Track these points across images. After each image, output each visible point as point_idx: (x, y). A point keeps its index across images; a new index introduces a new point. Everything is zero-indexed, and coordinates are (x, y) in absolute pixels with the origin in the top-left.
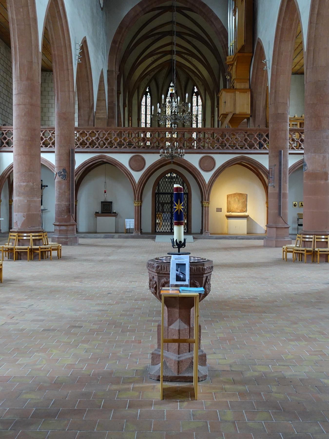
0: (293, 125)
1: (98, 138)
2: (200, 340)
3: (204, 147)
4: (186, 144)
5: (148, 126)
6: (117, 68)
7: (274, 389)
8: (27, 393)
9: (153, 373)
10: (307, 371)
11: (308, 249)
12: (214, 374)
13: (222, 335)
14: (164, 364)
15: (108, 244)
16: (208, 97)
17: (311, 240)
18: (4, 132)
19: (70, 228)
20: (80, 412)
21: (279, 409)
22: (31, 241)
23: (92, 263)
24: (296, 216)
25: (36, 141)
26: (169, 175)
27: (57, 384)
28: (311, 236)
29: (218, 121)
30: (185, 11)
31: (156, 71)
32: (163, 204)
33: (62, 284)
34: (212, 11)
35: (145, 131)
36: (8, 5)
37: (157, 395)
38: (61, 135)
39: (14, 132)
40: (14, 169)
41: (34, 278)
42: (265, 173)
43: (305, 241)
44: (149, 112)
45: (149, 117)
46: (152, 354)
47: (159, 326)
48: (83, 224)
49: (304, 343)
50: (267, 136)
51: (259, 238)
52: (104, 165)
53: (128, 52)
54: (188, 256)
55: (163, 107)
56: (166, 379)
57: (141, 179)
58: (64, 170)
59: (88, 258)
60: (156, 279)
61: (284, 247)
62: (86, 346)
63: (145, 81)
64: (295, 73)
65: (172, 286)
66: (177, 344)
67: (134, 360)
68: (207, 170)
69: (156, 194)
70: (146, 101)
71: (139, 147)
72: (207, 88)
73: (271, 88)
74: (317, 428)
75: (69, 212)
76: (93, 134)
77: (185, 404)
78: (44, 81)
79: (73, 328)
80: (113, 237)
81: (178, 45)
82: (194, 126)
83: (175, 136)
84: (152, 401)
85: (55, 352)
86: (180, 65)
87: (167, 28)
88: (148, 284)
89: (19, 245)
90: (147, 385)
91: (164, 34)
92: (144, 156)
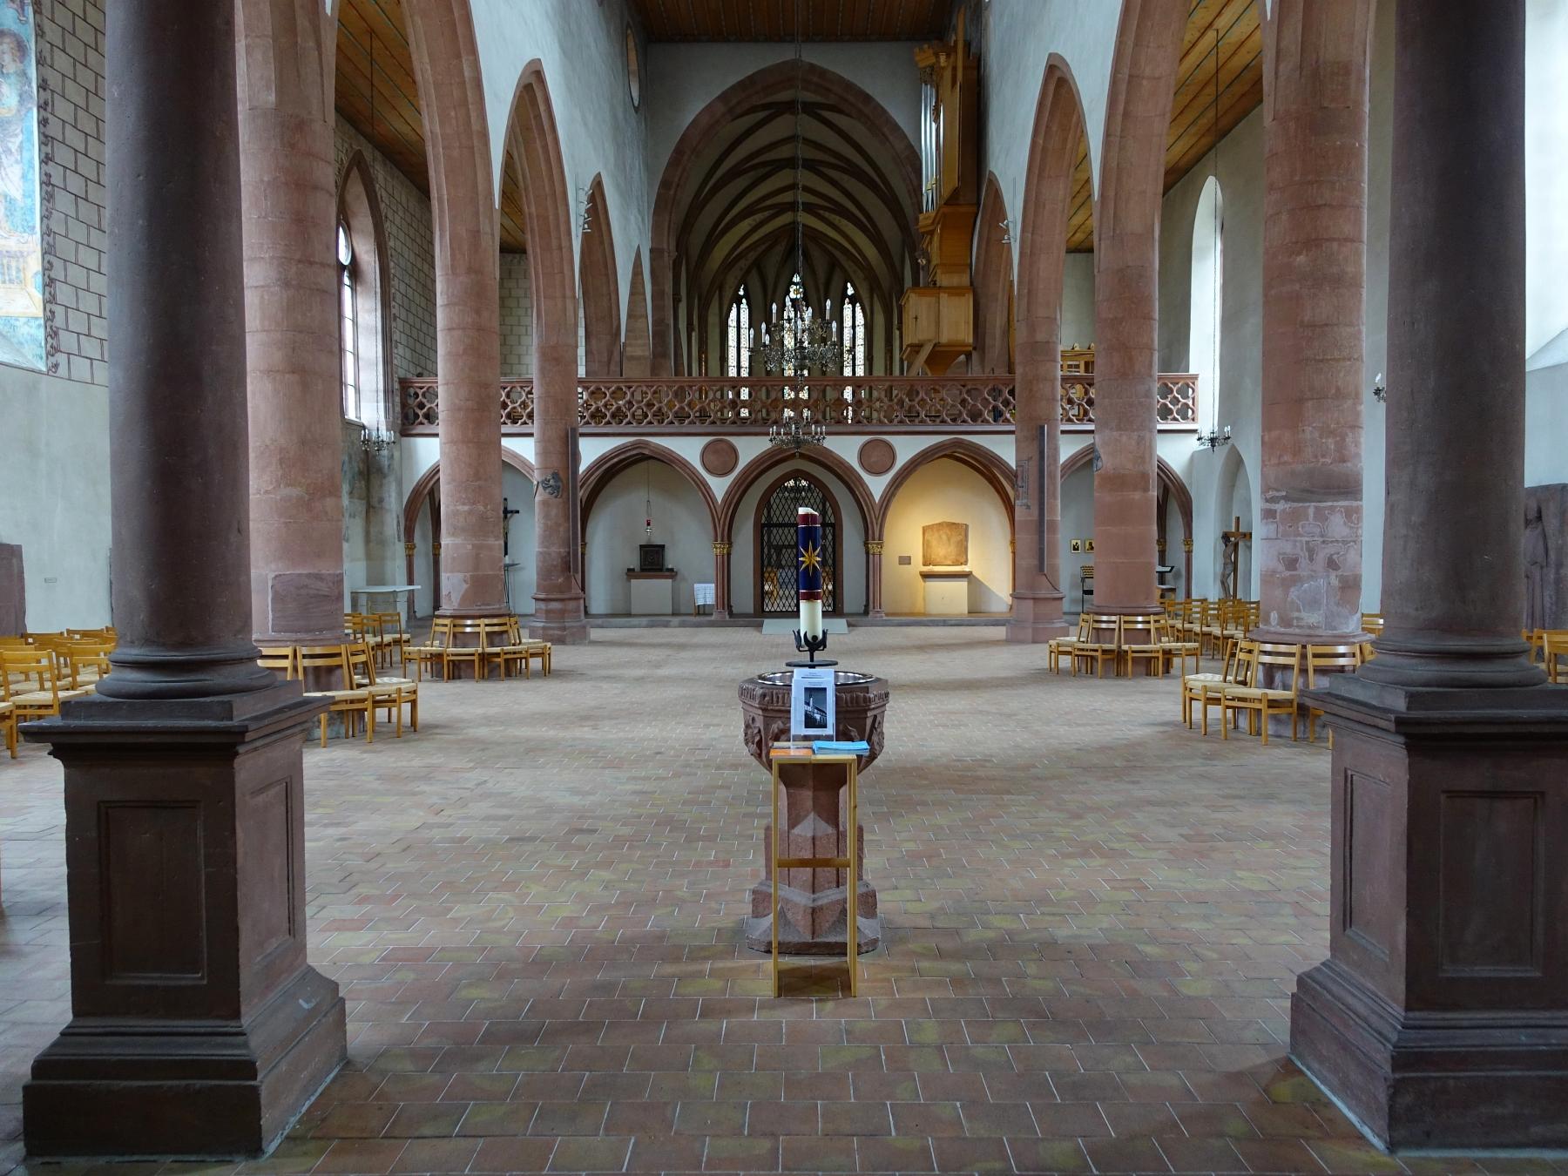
1: (630, 402)
2: (860, 859)
3: (869, 419)
4: (829, 413)
5: (745, 374)
7: (1032, 969)
8: (470, 985)
9: (755, 935)
10: (1105, 925)
11: (1107, 646)
12: (895, 935)
13: (911, 846)
14: (781, 915)
15: (656, 640)
16: (878, 307)
17: (1112, 626)
19: (571, 605)
20: (590, 1028)
21: (1044, 1015)
22: (483, 638)
23: (619, 685)
24: (1079, 573)
25: (488, 413)
26: (792, 483)
27: (540, 964)
28: (1113, 618)
29: (902, 361)
30: (827, 114)
31: (760, 250)
32: (779, 549)
33: (552, 733)
34: (884, 111)
35: (736, 384)
36: (423, 103)
37: (766, 987)
38: (547, 396)
39: (441, 391)
40: (441, 474)
41: (488, 721)
42: (1007, 477)
43: (1098, 629)
44: (744, 343)
45: (745, 355)
46: (754, 892)
47: (768, 829)
48: (600, 595)
49: (1097, 862)
50: (1012, 393)
51: (996, 623)
52: (643, 465)
53: (697, 206)
54: (831, 670)
55: (775, 330)
56: (786, 949)
57: (729, 493)
58: (555, 476)
59: (611, 672)
60: (759, 723)
61: (1052, 642)
62: (605, 875)
63: (736, 274)
64: (1073, 250)
65: (796, 738)
66: (809, 870)
67: (714, 905)
68: (877, 472)
69: (763, 526)
70: (739, 317)
71: (724, 421)
72: (874, 284)
73: (1020, 282)
74: (1129, 1059)
75: (568, 568)
76: (619, 394)
77: (830, 1005)
78: (507, 274)
79: (577, 832)
80: (666, 625)
81: (806, 189)
82: (847, 372)
83: (804, 395)
85: (535, 889)
86: (813, 235)
87: (784, 152)
88: (741, 736)
89: (455, 646)
90: (743, 963)
92: (736, 441)
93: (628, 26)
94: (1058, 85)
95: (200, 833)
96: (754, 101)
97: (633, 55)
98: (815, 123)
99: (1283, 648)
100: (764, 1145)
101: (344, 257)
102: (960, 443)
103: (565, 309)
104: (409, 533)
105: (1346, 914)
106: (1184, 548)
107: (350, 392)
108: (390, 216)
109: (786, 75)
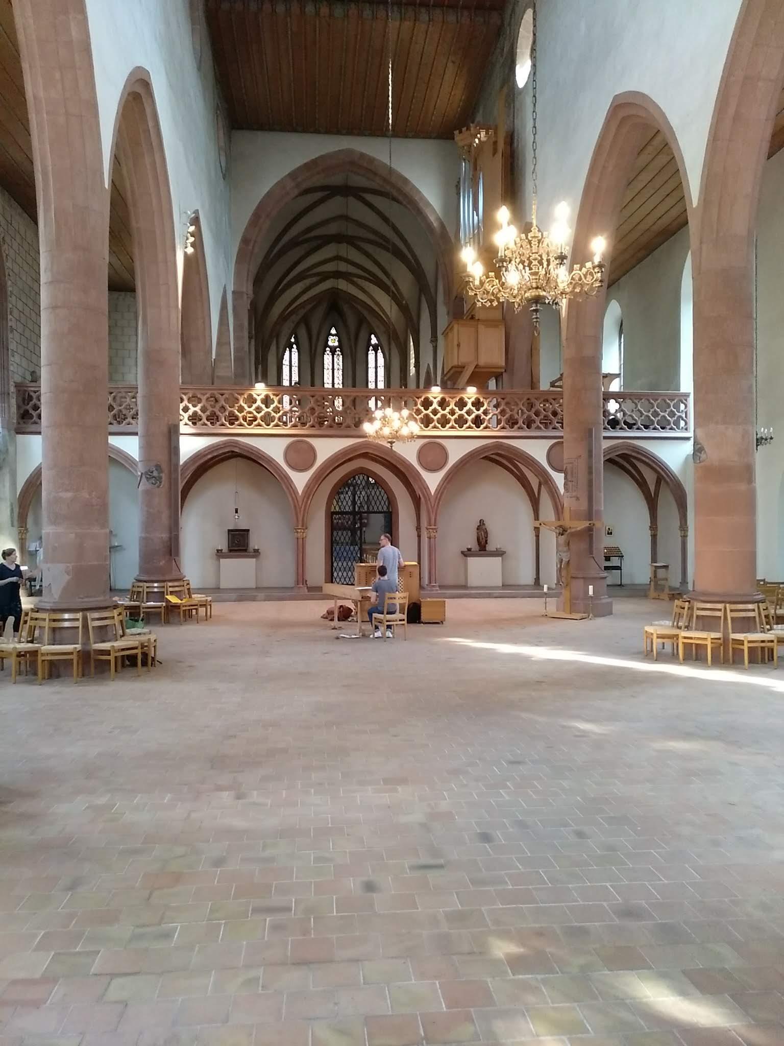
17: (751, 614)
18: (32, 394)
28: (750, 606)
52: (233, 461)
68: (432, 468)
78: (113, 308)
87: (332, 229)
98: (360, 205)
99: (709, 606)
102: (501, 446)
103: (169, 316)
106: (679, 533)
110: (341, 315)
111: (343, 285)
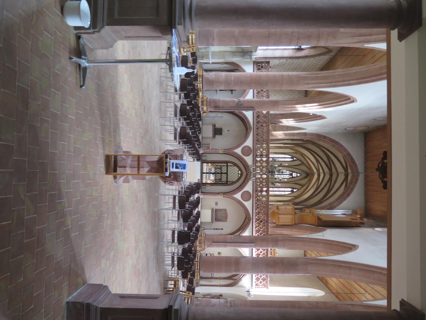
0: (271, 252)
6: (308, 139)
13: (139, 196)
28: (199, 260)
37: (107, 153)
40: (243, 73)
49: (133, 244)
53: (319, 146)
57: (236, 153)
58: (242, 104)
62: (134, 115)
63: (300, 157)
68: (242, 196)
84: (63, 199)
86: (310, 181)
87: (334, 170)
91: (330, 169)
93: (369, 127)
94: (350, 248)
95: (151, 17)
96: (349, 163)
97: (361, 128)
100: (72, 150)
101: (303, 47)
104: (226, 63)
105: (123, 297)
107: (266, 48)
108: (315, 59)
109: (358, 173)
110: (305, 177)
111: (316, 176)
